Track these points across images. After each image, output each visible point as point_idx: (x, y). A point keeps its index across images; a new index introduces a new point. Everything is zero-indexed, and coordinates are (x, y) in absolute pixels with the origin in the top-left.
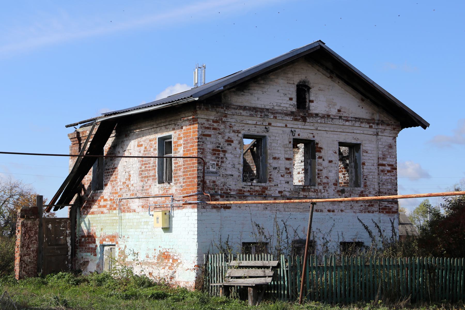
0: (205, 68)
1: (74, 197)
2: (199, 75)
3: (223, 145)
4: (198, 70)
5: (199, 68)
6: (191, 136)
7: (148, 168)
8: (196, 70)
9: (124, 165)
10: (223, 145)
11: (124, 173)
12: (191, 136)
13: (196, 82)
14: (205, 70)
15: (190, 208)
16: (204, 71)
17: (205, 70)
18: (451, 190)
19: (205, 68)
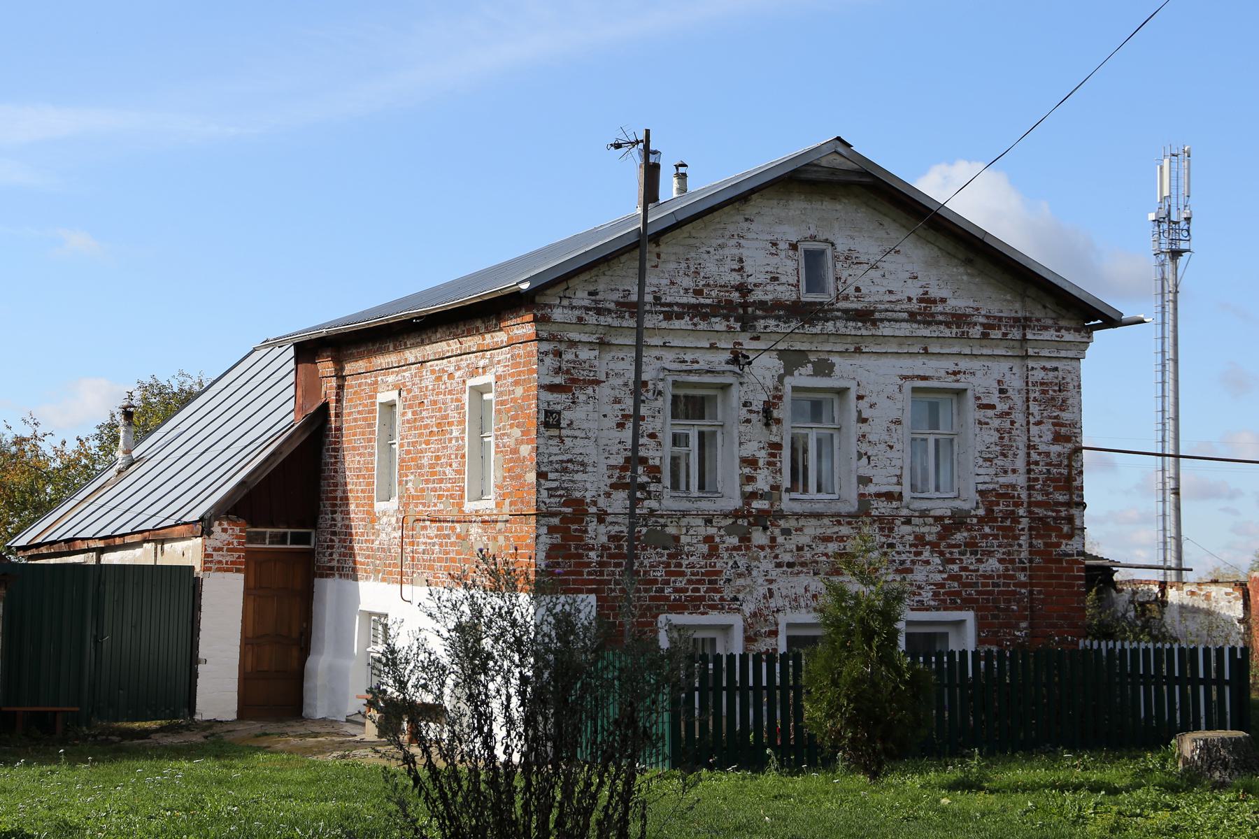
0: (1189, 156)
1: (77, 561)
2: (1174, 174)
3: (652, 436)
4: (1170, 162)
5: (1173, 155)
6: (654, 589)
7: (434, 508)
8: (1166, 162)
9: (1219, 600)
10: (652, 436)
11: (687, 282)
12: (654, 589)
13: (1166, 193)
14: (1189, 161)
15: (874, 229)
16: (1186, 163)
17: (1189, 161)
18: (1034, 377)
19: (1189, 156)
